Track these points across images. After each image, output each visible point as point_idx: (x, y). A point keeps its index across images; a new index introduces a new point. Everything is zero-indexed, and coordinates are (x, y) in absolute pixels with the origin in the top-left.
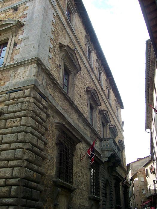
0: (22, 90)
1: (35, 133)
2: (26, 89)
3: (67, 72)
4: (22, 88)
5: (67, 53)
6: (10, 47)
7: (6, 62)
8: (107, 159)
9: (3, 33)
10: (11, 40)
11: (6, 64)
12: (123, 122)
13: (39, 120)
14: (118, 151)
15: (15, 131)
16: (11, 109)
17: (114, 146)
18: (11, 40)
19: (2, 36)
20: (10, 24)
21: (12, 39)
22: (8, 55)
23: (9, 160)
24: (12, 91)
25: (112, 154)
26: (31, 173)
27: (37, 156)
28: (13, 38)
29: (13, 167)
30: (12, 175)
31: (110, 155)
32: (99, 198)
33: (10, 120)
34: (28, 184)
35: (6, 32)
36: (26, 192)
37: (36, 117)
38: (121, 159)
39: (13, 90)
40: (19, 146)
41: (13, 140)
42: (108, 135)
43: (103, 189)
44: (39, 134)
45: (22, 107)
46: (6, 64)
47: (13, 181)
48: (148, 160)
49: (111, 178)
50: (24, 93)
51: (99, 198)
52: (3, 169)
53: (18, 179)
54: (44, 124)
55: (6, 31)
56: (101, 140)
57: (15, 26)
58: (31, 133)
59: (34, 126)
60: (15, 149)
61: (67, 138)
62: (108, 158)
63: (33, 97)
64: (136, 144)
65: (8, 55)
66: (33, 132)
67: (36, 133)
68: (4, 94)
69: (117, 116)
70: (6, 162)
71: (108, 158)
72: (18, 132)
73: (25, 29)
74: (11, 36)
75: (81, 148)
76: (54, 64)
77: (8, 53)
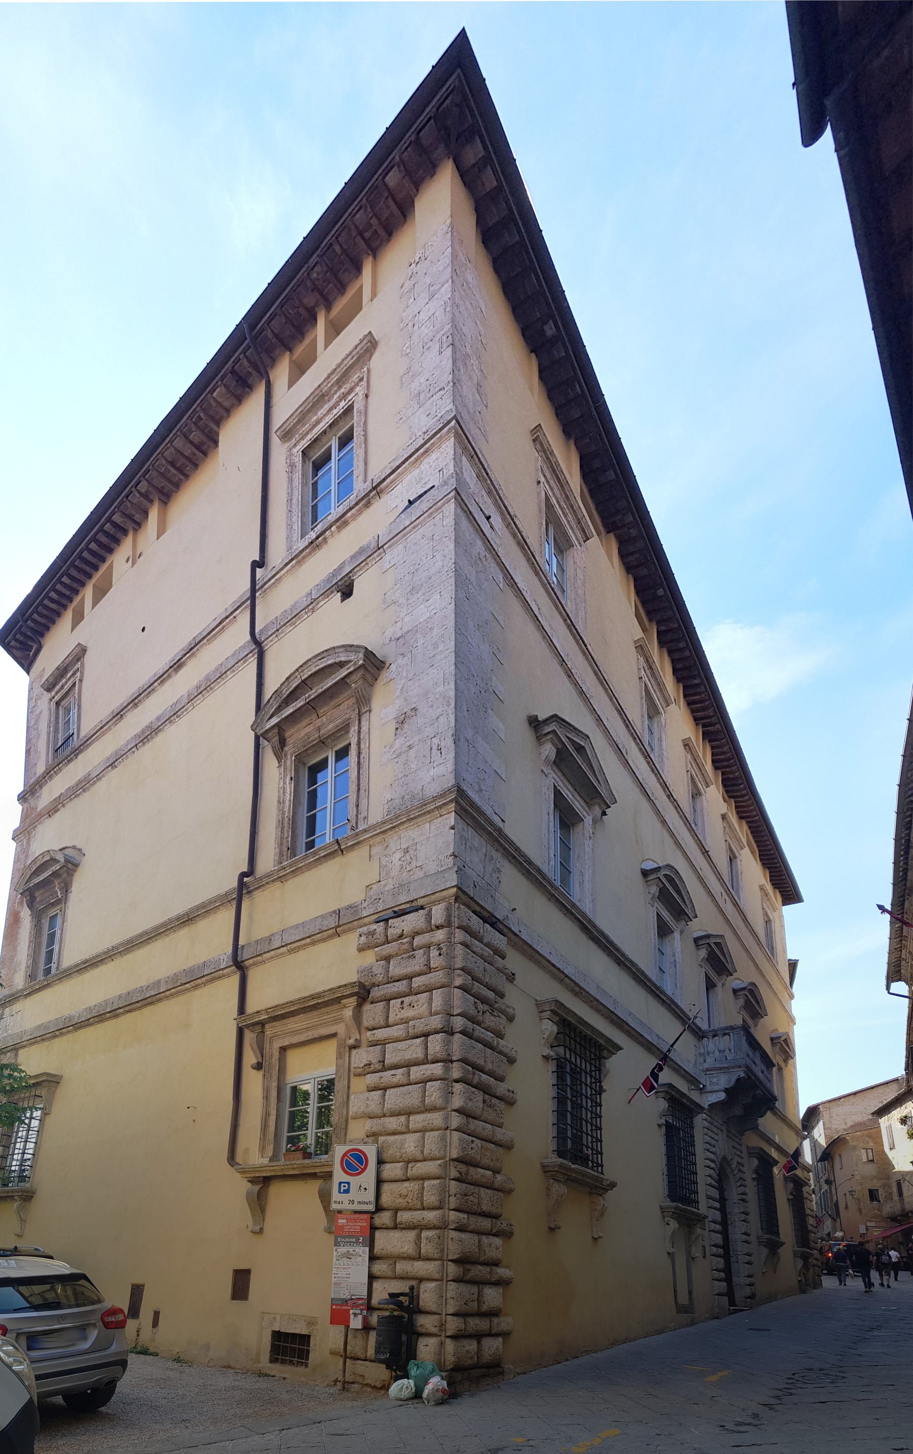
0: (422, 908)
1: (477, 1033)
2: (434, 903)
3: (567, 819)
4: (421, 902)
5: (560, 746)
6: (359, 757)
7: (357, 816)
8: (722, 1096)
9: (325, 709)
10: (359, 732)
11: (357, 823)
12: (793, 966)
13: (484, 993)
14: (763, 1068)
15: (418, 1031)
16: (396, 969)
17: (750, 1053)
18: (359, 732)
19: (324, 719)
20: (341, 665)
21: (360, 728)
22: (359, 790)
23: (409, 1113)
24: (393, 915)
25: (738, 1080)
26: (473, 1145)
27: (487, 1097)
28: (363, 723)
29: (423, 1131)
30: (422, 1152)
31: (732, 1084)
32: (696, 1210)
33: (400, 1000)
34: (467, 1174)
35: (333, 703)
36: (466, 1195)
37: (473, 985)
38: (776, 1093)
39: (396, 909)
40: (435, 1072)
41: (414, 1056)
42: (729, 1012)
43: (762, 831)
44: (489, 1036)
45: (429, 960)
46: (357, 823)
47: (431, 1167)
48: (891, 1094)
49: (739, 1153)
50: (429, 916)
51: (696, 1210)
52: (397, 1137)
53: (440, 1162)
54: (501, 1004)
55: (332, 697)
56: (699, 1034)
57: (361, 672)
58: (463, 1032)
59: (472, 1011)
60: (424, 1082)
61: (572, 1035)
62: (726, 1091)
63: (458, 928)
64: (834, 1045)
65: (359, 790)
66: (471, 1031)
67: (479, 1032)
68: (370, 924)
69: (768, 942)
70: (403, 1119)
71: (726, 1091)
72: (426, 1035)
73: (397, 671)
74: (354, 715)
75: (626, 1069)
76: (525, 805)
77: (359, 785)
